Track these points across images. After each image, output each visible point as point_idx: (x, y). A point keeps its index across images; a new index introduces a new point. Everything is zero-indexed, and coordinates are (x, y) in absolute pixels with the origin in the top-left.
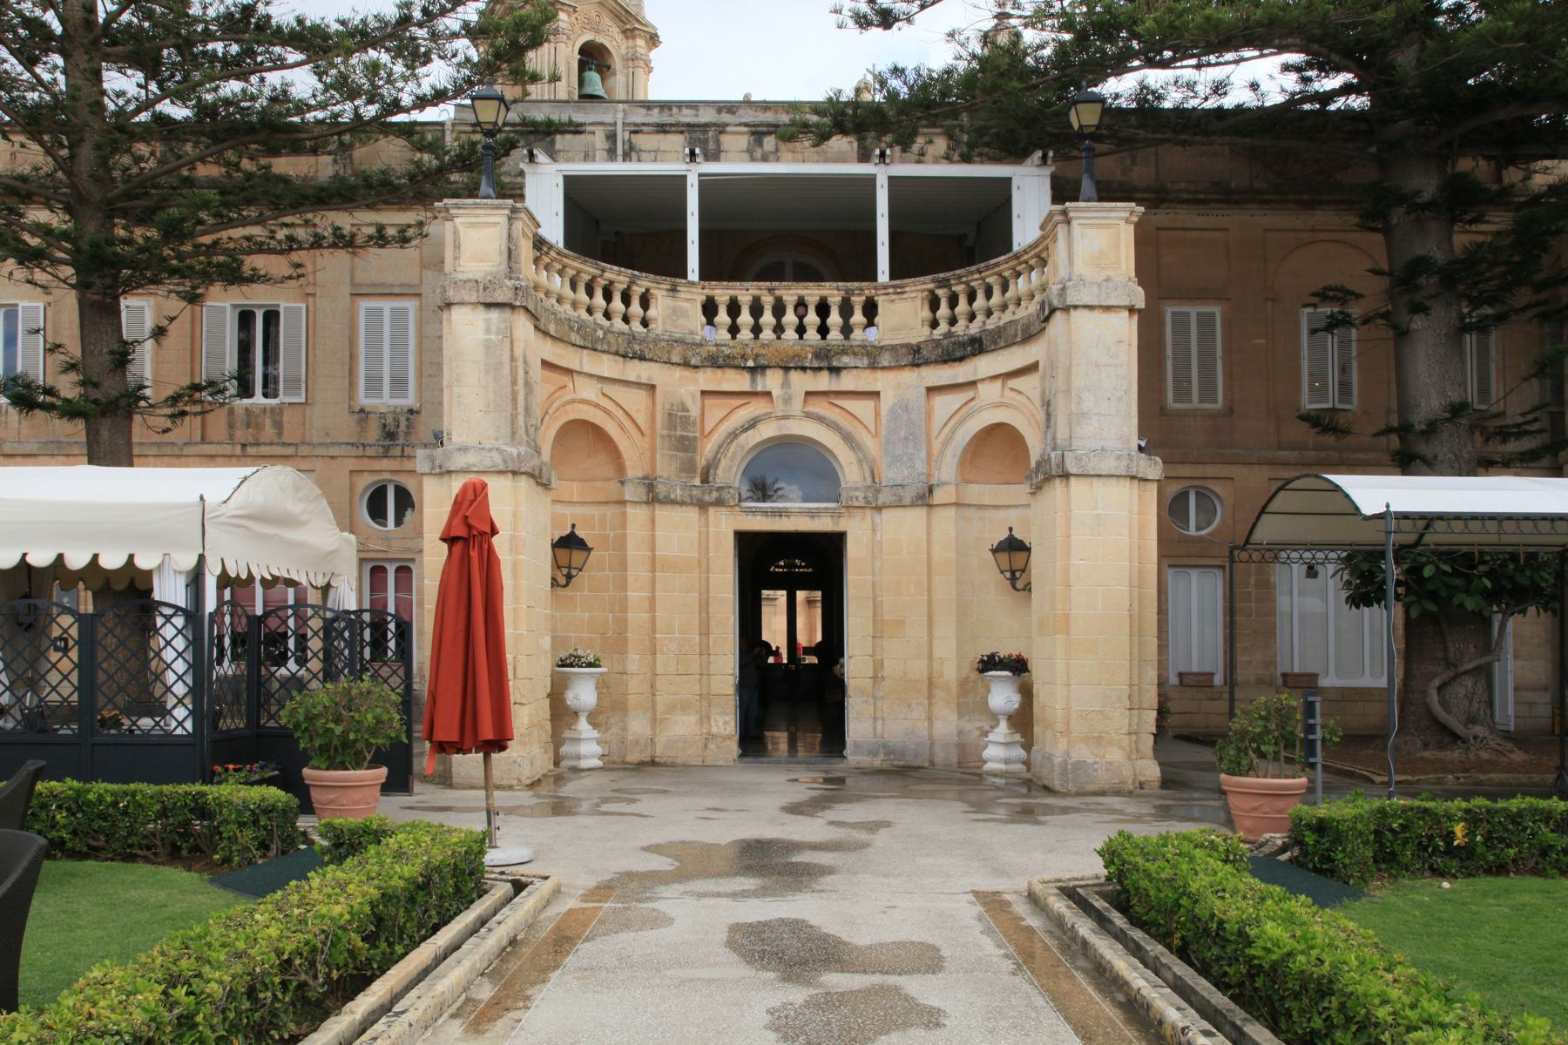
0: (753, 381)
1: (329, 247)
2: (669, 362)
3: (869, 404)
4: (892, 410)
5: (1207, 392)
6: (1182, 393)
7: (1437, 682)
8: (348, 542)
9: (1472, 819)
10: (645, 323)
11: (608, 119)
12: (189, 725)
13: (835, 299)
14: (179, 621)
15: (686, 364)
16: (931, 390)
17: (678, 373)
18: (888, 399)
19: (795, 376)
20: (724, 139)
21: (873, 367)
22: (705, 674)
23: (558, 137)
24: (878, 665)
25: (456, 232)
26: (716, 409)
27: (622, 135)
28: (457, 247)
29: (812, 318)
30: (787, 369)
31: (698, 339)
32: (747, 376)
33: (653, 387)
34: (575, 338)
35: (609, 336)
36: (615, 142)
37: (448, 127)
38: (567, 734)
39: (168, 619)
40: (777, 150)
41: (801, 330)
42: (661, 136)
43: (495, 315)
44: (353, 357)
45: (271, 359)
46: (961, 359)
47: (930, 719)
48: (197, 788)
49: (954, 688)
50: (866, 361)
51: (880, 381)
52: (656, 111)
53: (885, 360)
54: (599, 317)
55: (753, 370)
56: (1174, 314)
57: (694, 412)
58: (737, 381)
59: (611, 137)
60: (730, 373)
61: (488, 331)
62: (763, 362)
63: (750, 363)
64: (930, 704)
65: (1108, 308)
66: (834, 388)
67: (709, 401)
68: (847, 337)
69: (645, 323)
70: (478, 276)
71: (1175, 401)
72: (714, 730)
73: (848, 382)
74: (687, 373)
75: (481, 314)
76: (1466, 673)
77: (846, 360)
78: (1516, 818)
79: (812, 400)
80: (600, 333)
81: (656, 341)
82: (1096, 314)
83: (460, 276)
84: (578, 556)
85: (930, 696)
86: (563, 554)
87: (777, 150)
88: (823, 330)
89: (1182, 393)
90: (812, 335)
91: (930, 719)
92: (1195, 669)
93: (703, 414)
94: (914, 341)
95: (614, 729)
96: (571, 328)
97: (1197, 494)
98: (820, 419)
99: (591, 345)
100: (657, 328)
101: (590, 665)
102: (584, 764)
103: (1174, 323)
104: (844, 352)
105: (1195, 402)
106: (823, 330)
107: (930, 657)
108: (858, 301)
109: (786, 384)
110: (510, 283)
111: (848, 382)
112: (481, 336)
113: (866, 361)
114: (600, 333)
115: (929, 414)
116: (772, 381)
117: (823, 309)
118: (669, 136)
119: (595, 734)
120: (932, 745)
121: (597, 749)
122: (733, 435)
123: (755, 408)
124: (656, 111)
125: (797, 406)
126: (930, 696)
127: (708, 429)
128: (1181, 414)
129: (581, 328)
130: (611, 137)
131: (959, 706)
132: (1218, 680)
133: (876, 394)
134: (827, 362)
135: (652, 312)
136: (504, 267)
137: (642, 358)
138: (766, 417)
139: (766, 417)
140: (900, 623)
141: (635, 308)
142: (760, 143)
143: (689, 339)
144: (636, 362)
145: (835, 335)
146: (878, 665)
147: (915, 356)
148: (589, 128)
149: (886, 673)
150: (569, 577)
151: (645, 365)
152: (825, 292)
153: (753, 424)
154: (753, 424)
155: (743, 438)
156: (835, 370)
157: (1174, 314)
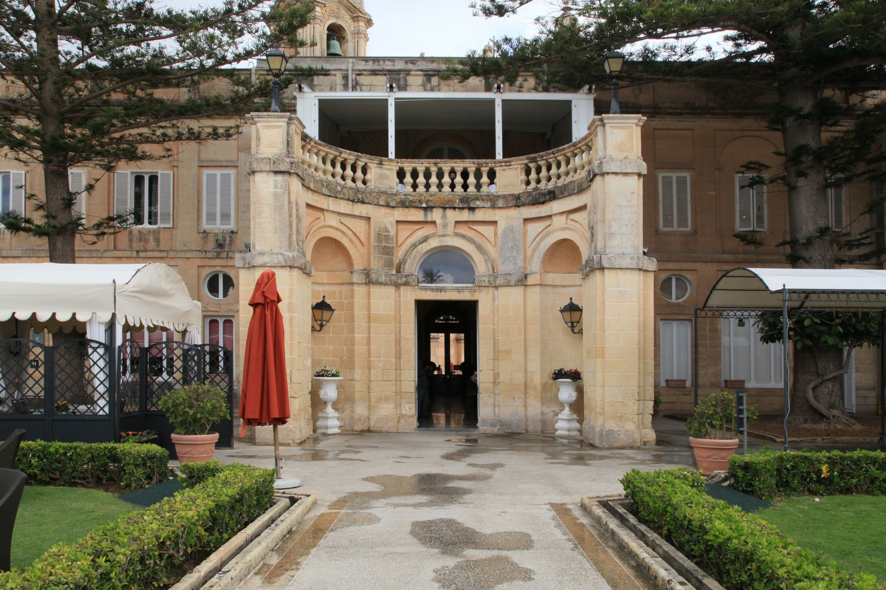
0: (426, 215)
1: (186, 139)
2: (378, 205)
3: (491, 228)
4: (504, 232)
5: (682, 222)
6: (668, 222)
7: (812, 385)
8: (197, 306)
9: (832, 462)
10: (364, 182)
11: (344, 67)
12: (107, 409)
13: (472, 169)
14: (101, 351)
15: (388, 206)
16: (526, 220)
17: (383, 210)
18: (502, 226)
19: (449, 212)
20: (409, 78)
21: (493, 207)
22: (398, 381)
23: (315, 78)
24: (496, 376)
25: (257, 131)
26: (405, 231)
27: (351, 76)
28: (258, 139)
29: (459, 180)
30: (445, 208)
31: (394, 191)
32: (422, 212)
33: (369, 219)
34: (325, 191)
35: (344, 190)
36: (347, 80)
37: (253, 72)
38: (320, 414)
39: (95, 349)
40: (439, 85)
41: (453, 186)
42: (374, 77)
43: (279, 178)
44: (199, 202)
45: (153, 203)
46: (543, 203)
47: (525, 406)
48: (111, 445)
49: (539, 388)
50: (489, 204)
51: (497, 215)
52: (371, 62)
53: (500, 203)
54: (338, 179)
55: (425, 209)
56: (663, 177)
57: (392, 232)
58: (416, 215)
59: (345, 77)
60: (413, 211)
61: (276, 187)
62: (431, 204)
63: (424, 205)
64: (526, 397)
65: (626, 174)
66: (471, 219)
67: (400, 227)
68: (479, 190)
69: (364, 182)
70: (270, 156)
71: (664, 227)
72: (404, 412)
73: (479, 215)
74: (388, 211)
75: (272, 177)
76: (828, 380)
77: (478, 203)
78: (856, 462)
79: (459, 226)
80: (339, 188)
81: (371, 193)
82: (619, 177)
83: (260, 156)
84: (326, 314)
85: (526, 393)
86: (318, 313)
87: (439, 85)
88: (465, 187)
89: (668, 222)
90: (459, 189)
91: (525, 406)
92: (675, 378)
93: (397, 234)
94: (516, 193)
95: (347, 412)
96: (323, 185)
97: (677, 279)
98: (463, 237)
99: (334, 195)
100: (371, 185)
101: (333, 375)
102: (330, 431)
103: (663, 182)
104: (477, 199)
105: (675, 227)
106: (465, 187)
107: (526, 371)
108: (485, 170)
109: (444, 217)
110: (288, 160)
111: (479, 215)
112: (272, 190)
113: (489, 204)
114: (339, 188)
115: (525, 234)
116: (436, 215)
117: (465, 175)
118: (378, 77)
119: (336, 414)
120: (527, 420)
121: (338, 423)
122: (414, 246)
123: (427, 230)
124: (371, 62)
125: (450, 229)
126: (526, 393)
127: (400, 242)
128: (667, 234)
129: (329, 185)
130: (345, 77)
131: (542, 399)
132: (688, 384)
133: (495, 223)
134: (467, 205)
135: (368, 176)
136: (285, 151)
137: (363, 202)
138: (433, 235)
139: (433, 235)
140: (509, 352)
141: (359, 174)
142: (429, 81)
143: (389, 191)
144: (359, 204)
145: (472, 189)
146: (496, 376)
147: (517, 201)
148: (333, 72)
149: (501, 380)
150: (322, 326)
151: (364, 206)
152: (466, 165)
153: (425, 239)
154: (425, 239)
155: (420, 247)
156: (472, 209)
157: (663, 177)
